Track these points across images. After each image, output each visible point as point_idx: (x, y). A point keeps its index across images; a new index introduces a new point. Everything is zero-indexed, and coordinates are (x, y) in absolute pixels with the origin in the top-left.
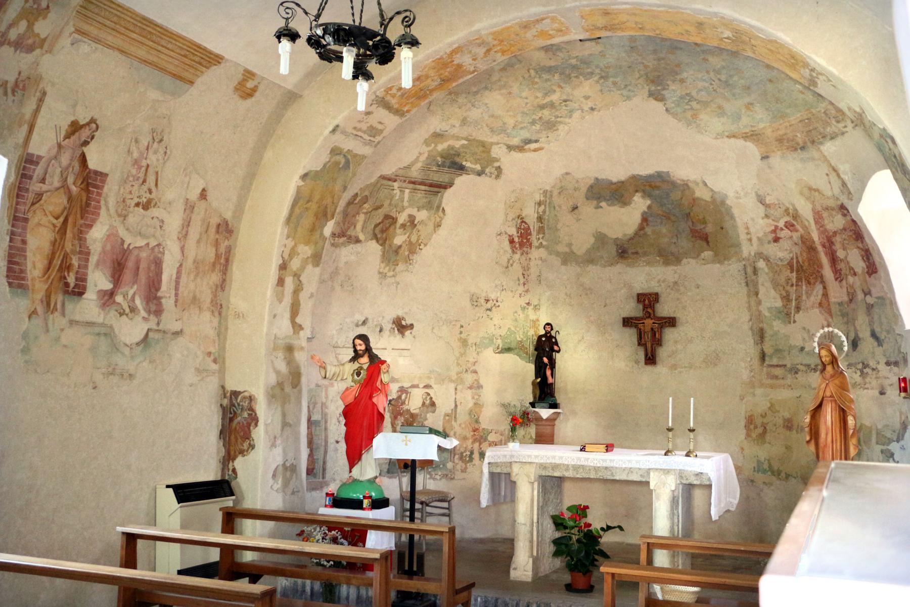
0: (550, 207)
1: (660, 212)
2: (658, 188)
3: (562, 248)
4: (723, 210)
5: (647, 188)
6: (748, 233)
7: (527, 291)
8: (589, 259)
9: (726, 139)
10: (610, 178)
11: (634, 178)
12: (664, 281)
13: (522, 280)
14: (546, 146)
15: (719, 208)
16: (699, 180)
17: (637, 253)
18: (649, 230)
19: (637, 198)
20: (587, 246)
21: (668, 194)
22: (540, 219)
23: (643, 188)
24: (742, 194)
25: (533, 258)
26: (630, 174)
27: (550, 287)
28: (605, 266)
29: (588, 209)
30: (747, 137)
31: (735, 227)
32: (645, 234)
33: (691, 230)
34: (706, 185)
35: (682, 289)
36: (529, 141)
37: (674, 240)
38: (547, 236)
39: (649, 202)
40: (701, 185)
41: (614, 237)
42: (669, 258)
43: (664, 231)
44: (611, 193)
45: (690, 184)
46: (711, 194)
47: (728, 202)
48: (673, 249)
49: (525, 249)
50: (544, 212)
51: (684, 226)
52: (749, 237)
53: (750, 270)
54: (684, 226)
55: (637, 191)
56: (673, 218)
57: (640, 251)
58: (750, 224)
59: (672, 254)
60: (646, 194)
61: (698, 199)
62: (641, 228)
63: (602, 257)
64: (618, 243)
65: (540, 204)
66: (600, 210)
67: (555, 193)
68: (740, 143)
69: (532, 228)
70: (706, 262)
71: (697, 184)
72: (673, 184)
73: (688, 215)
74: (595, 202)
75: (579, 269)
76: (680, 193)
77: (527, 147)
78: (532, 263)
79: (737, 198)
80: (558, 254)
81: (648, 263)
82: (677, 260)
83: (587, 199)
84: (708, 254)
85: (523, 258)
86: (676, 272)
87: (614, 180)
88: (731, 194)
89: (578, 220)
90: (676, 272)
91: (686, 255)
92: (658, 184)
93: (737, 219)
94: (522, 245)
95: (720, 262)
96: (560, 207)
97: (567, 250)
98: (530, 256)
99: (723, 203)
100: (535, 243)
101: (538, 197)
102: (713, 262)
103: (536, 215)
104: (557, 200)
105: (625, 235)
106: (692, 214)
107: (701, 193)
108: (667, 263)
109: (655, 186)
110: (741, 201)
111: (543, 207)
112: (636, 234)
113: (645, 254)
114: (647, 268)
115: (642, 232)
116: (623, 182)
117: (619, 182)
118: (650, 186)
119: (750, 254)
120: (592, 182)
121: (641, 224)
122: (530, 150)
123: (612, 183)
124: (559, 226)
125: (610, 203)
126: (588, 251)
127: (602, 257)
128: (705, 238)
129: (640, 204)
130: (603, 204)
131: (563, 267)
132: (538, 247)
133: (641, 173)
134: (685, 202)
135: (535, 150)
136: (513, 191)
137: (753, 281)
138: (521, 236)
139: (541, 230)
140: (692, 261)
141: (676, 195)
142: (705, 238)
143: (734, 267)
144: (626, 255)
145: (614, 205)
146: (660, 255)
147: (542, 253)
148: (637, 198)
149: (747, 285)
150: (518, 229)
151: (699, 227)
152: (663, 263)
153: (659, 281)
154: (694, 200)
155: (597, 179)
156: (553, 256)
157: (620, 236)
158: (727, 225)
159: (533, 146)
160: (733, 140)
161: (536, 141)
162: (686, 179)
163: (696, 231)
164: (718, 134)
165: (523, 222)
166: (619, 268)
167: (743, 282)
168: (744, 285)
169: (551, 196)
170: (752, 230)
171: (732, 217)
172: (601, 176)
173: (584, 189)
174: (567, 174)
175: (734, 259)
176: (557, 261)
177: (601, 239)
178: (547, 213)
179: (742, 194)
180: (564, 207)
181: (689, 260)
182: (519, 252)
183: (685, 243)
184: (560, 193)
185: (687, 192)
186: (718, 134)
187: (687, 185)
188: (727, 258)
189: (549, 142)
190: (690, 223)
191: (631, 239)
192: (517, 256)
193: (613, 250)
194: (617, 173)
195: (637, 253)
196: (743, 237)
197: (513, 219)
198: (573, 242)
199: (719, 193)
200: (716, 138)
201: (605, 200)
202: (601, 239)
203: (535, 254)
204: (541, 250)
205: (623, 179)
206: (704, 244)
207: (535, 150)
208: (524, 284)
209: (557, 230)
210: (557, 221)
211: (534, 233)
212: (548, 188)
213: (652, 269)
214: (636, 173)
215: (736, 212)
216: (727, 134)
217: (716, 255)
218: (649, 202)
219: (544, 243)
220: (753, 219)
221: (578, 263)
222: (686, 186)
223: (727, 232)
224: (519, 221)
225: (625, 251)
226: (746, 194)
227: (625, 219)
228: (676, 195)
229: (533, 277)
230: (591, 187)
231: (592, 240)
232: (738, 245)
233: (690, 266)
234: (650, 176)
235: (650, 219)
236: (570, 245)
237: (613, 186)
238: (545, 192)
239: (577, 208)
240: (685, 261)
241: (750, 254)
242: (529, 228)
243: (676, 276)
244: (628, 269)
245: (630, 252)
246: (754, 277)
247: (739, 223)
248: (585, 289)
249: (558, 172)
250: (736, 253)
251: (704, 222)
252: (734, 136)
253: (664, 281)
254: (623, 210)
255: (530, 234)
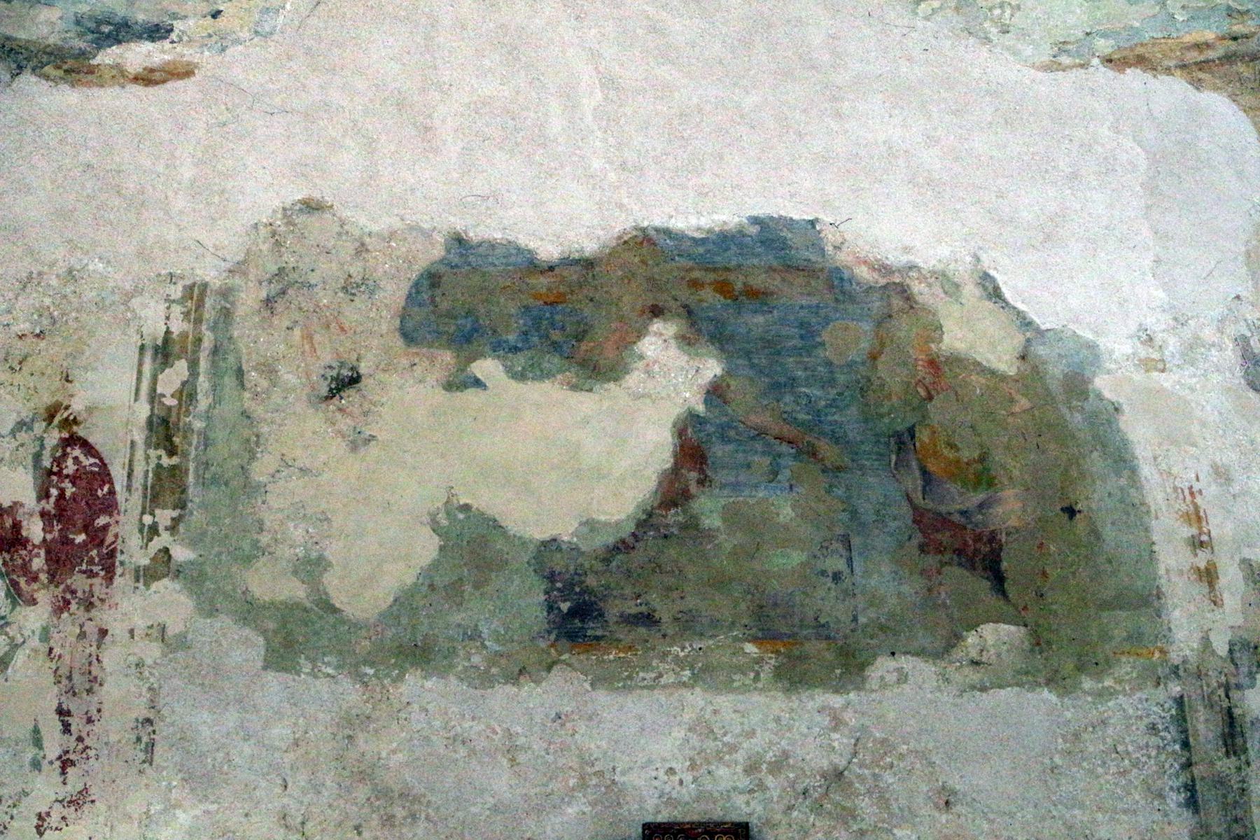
0: (216, 373)
1: (761, 419)
2: (1194, 445)
3: (271, 583)
4: (1076, 420)
5: (709, 296)
6: (1198, 544)
7: (78, 801)
8: (408, 643)
9: (1102, 75)
10: (523, 241)
11: (645, 243)
12: (777, 767)
13: (54, 744)
14: (205, 58)
15: (1057, 412)
16: (962, 270)
17: (648, 619)
18: (709, 508)
19: (658, 345)
20: (399, 575)
21: (808, 333)
22: (164, 430)
23: (684, 295)
24: (1173, 345)
25: (117, 629)
26: (622, 224)
27: (202, 780)
28: (485, 680)
29: (408, 392)
30: (1202, 65)
31: (1134, 511)
32: (692, 526)
33: (919, 517)
34: (995, 294)
35: (866, 807)
36: (119, 31)
37: (837, 563)
38: (197, 517)
39: (712, 368)
40: (970, 291)
41: (540, 535)
42: (808, 647)
43: (786, 513)
44: (520, 312)
45: (917, 288)
46: (1018, 340)
47: (1102, 384)
48: (828, 604)
49: (79, 581)
50: (187, 394)
51: (881, 490)
52: (1202, 560)
53: (1205, 727)
54: (881, 490)
55: (656, 312)
56: (827, 450)
57: (664, 613)
58: (1211, 491)
59: (822, 630)
60: (701, 330)
61: (956, 360)
62: (673, 493)
63: (473, 636)
64: (558, 563)
65: (164, 352)
66: (374, 450)
67: (249, 298)
68: (1170, 91)
69: (118, 473)
70: (987, 672)
71: (952, 288)
72: (838, 285)
73: (903, 441)
74: (447, 357)
75: (351, 694)
76: (867, 327)
77: (107, 57)
78: (112, 658)
79: (1147, 365)
80: (250, 612)
81: (704, 674)
82: (849, 665)
83: (409, 336)
84: (996, 637)
85: (68, 626)
86: (837, 723)
87: (548, 251)
88: (1118, 346)
89: (359, 442)
90: (837, 723)
91: (892, 635)
92: (759, 281)
93: (1146, 471)
94: (61, 559)
95: (1054, 680)
96: (269, 370)
97: (295, 590)
98: (103, 616)
99: (1077, 385)
100: (135, 552)
101: (156, 317)
102: (1025, 678)
103: (143, 410)
104: (253, 338)
105: (591, 525)
106: (923, 436)
107: (973, 336)
108: (794, 675)
109: (748, 290)
110: (1166, 381)
111: (180, 369)
112: (646, 522)
113: (688, 624)
114: (696, 698)
115: (674, 517)
116: (588, 264)
117: (567, 262)
118: (723, 288)
119: (1206, 642)
120: (438, 252)
121: (676, 471)
122: (120, 76)
123: (533, 266)
124: (260, 471)
125: (520, 361)
126: (404, 603)
127: (473, 636)
128: (985, 558)
129: (670, 375)
130: (487, 368)
131: (273, 679)
132: (147, 575)
133: (678, 224)
134: (892, 376)
135: (148, 78)
136: (26, 283)
137: (1220, 782)
138: (59, 515)
139: (166, 487)
140: (922, 670)
141: (848, 339)
142: (985, 558)
143: (1127, 709)
144: (593, 629)
145: (544, 375)
146: (766, 636)
147: (169, 602)
148: (658, 345)
149: (1192, 803)
150: (47, 478)
151: (958, 499)
152: (778, 674)
153: (751, 769)
154: (933, 363)
155: (459, 241)
156: (224, 622)
157: (565, 530)
158: (1097, 497)
159: (138, 55)
160: (1134, 78)
161: (156, 32)
162: (895, 258)
163: (944, 521)
164: (1062, 47)
165: (73, 440)
166: (561, 689)
167: (1172, 782)
168: (1175, 799)
169: (226, 315)
170: (1220, 527)
171: (1122, 460)
172: (483, 229)
173: (394, 293)
174: (312, 207)
175: (1126, 668)
176: (243, 648)
177: (472, 544)
178: (203, 402)
179: (1173, 345)
180: (288, 376)
181: (906, 662)
182: (45, 597)
183: (885, 580)
184: (269, 302)
185: (904, 329)
186: (1062, 47)
187: (904, 292)
188: (1090, 661)
189: (222, 43)
190: (913, 481)
191: (622, 547)
192: (33, 619)
193: (530, 601)
194: (561, 214)
195: (648, 619)
196: (1173, 559)
197: (22, 425)
198: (333, 551)
199: (1058, 335)
200: (1052, 66)
201: (500, 348)
202: (472, 544)
203: (132, 608)
204: (165, 586)
205: (590, 247)
206: (981, 586)
207: (148, 78)
208: (66, 763)
209: (251, 489)
210: (252, 447)
211: (130, 502)
212: (210, 273)
213: (724, 702)
214: (655, 218)
215: (1139, 432)
216: (1104, 46)
217: (1038, 642)
218: (712, 368)
219: (181, 554)
220: (1222, 474)
221: (353, 666)
222: (896, 294)
223: (1096, 533)
224: (54, 437)
225: (590, 609)
226: (1192, 350)
227: (590, 450)
228: (848, 339)
229: (114, 728)
230: (433, 278)
231: (427, 547)
232: (1148, 600)
233: (907, 696)
234: (725, 239)
235: (718, 451)
236: (312, 567)
237: (542, 282)
238: (195, 294)
239: (354, 380)
240: (883, 667)
241: (1206, 642)
242: (104, 475)
243: (840, 740)
244: (602, 697)
245: (613, 610)
246: (1226, 765)
247: (1156, 493)
248: (383, 793)
249: (263, 192)
250: (1136, 638)
251: (982, 476)
252: (1141, 61)
253: (777, 767)
254: (586, 403)
255: (109, 506)
